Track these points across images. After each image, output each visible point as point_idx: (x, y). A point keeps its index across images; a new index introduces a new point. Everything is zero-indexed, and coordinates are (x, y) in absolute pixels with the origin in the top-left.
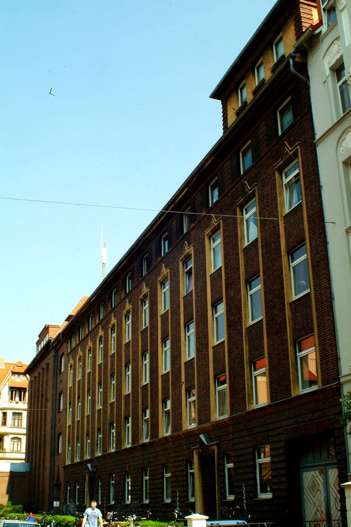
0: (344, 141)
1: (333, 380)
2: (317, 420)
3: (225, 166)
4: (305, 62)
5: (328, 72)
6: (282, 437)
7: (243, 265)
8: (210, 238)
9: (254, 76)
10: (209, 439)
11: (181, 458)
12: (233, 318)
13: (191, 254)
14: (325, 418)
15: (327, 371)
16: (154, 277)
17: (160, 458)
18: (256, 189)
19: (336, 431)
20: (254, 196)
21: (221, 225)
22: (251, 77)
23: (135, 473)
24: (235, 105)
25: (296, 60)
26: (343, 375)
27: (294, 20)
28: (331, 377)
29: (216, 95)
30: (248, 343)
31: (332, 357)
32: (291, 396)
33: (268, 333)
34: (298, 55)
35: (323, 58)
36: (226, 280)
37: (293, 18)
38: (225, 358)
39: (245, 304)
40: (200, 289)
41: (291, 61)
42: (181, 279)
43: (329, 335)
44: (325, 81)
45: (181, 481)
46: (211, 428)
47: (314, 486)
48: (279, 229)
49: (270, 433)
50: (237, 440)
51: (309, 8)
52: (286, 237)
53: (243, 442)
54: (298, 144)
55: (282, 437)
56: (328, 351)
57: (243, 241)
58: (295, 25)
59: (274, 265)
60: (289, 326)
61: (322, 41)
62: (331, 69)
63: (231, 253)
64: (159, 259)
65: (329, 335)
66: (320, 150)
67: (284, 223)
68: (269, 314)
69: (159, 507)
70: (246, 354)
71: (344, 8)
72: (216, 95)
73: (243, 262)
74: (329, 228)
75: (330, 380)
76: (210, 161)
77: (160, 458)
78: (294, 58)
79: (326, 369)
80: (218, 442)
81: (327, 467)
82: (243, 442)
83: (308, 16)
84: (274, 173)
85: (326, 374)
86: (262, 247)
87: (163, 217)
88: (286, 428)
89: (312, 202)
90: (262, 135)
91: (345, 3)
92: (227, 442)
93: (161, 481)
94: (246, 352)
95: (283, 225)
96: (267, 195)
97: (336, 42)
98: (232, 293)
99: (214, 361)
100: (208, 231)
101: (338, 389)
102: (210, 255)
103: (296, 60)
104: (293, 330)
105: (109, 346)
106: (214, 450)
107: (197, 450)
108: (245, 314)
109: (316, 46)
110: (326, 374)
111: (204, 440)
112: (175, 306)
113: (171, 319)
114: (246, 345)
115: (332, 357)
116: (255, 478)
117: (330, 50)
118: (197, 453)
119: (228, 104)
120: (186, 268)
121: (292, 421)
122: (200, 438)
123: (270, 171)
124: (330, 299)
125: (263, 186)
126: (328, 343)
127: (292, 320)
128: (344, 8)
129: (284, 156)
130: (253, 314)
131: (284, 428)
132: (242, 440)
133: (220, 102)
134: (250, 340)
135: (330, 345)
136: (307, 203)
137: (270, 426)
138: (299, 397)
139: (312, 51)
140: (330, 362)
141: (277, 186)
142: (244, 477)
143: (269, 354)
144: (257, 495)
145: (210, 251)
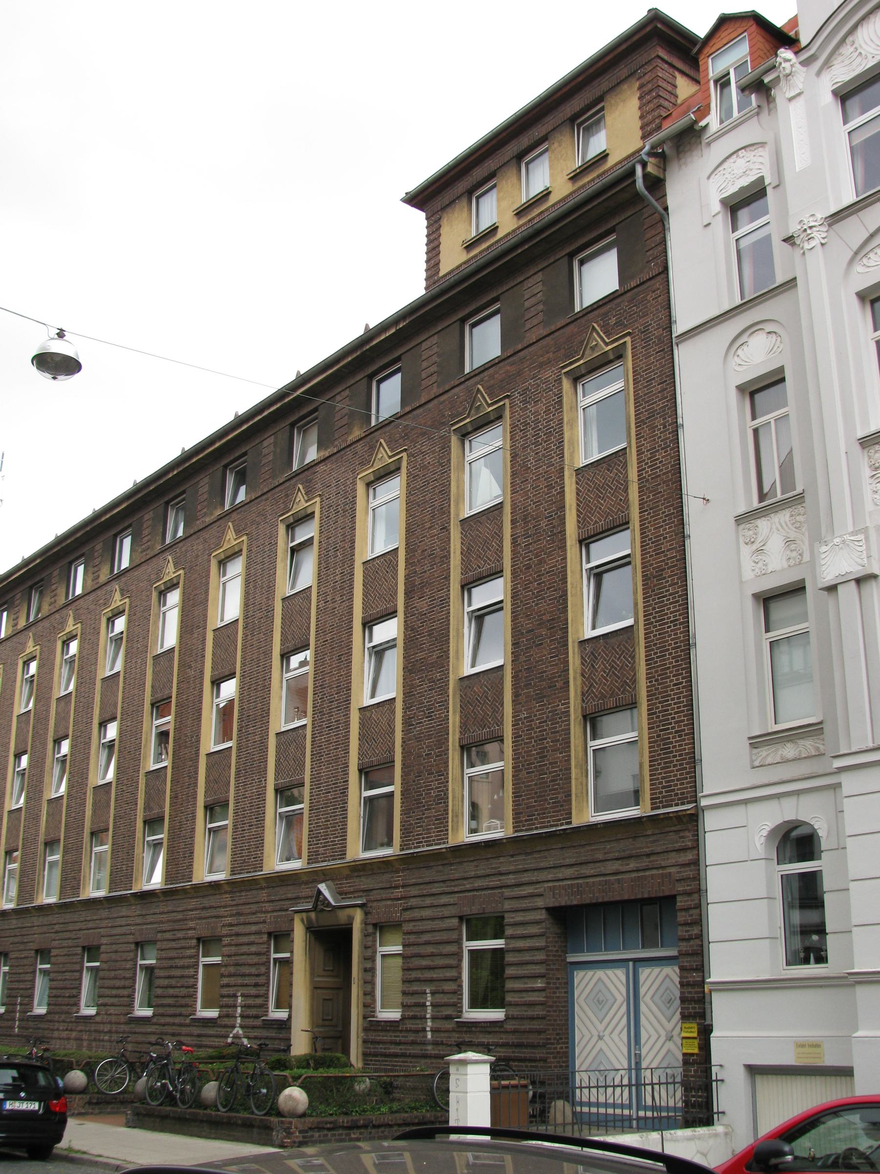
0: (744, 347)
1: (679, 799)
2: (634, 875)
3: (424, 346)
4: (662, 177)
5: (717, 207)
6: (540, 902)
7: (458, 552)
8: (368, 485)
9: (520, 180)
10: (341, 893)
11: (254, 928)
12: (421, 655)
13: (313, 513)
14: (654, 872)
15: (666, 782)
16: (201, 547)
17: (191, 924)
18: (508, 406)
19: (679, 898)
20: (500, 417)
21: (404, 464)
22: (514, 180)
23: (116, 952)
24: (458, 230)
25: (650, 169)
26: (705, 793)
27: (639, 89)
28: (676, 795)
29: (419, 199)
30: (458, 709)
31: (681, 755)
32: (570, 823)
33: (516, 695)
34: (652, 160)
35: (709, 178)
36: (407, 577)
37: (637, 84)
38: (393, 732)
39: (458, 630)
40: (334, 588)
41: (639, 170)
42: (279, 560)
43: (676, 713)
44: (709, 224)
45: (250, 975)
46: (346, 872)
47: (600, 1002)
48: (562, 493)
49: (507, 892)
50: (413, 902)
51: (671, 70)
52: (578, 510)
53: (432, 906)
54: (629, 334)
55: (540, 902)
56: (671, 743)
57: (461, 506)
58: (640, 98)
59: (541, 562)
60: (575, 685)
61: (709, 144)
62: (724, 202)
63: (428, 525)
64: (218, 512)
65: (676, 713)
66: (686, 358)
67: (577, 483)
68: (522, 658)
69: (181, 1025)
70: (454, 731)
71: (799, 94)
72: (419, 199)
73: (459, 546)
74: (692, 508)
75: (672, 800)
76: (393, 331)
77: (191, 924)
78: (644, 165)
79: (663, 778)
80: (364, 901)
81: (638, 964)
82: (432, 906)
83: (669, 88)
84: (559, 381)
85: (663, 787)
86: (513, 522)
87: (245, 427)
88: (550, 884)
89: (653, 452)
90: (533, 301)
91: (801, 86)
92: (389, 902)
93: (191, 971)
94: (454, 726)
95: (574, 486)
96: (537, 422)
97: (742, 153)
98: (422, 605)
99: (362, 737)
100: (368, 472)
101: (692, 821)
102: (366, 520)
103: (650, 169)
104: (583, 694)
105: (56, 679)
106: (351, 919)
107: (304, 915)
108: (457, 652)
109: (690, 150)
110: (663, 787)
111: (327, 893)
112: (259, 615)
113: (245, 639)
114: (454, 712)
115: (681, 755)
116: (458, 979)
117: (725, 165)
118: (302, 920)
119: (444, 222)
120: (292, 541)
121: (569, 872)
122: (319, 892)
123: (549, 374)
124: (685, 647)
125: (525, 402)
126: (673, 728)
127: (583, 675)
128: (799, 94)
129: (588, 352)
130: (481, 653)
131: (546, 885)
132: (428, 901)
133: (422, 215)
134: (465, 705)
135: (676, 732)
136: (639, 453)
137: (511, 879)
138: (592, 828)
139: (679, 159)
140: (675, 766)
141: (565, 407)
142: (434, 975)
143: (516, 737)
144: (461, 1012)
145: (367, 513)
